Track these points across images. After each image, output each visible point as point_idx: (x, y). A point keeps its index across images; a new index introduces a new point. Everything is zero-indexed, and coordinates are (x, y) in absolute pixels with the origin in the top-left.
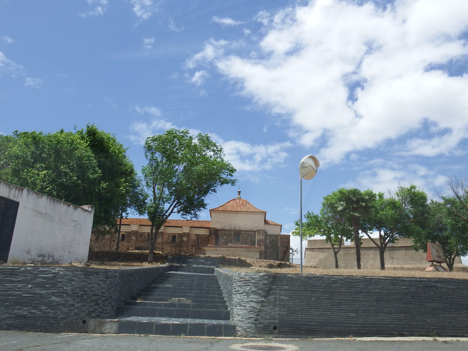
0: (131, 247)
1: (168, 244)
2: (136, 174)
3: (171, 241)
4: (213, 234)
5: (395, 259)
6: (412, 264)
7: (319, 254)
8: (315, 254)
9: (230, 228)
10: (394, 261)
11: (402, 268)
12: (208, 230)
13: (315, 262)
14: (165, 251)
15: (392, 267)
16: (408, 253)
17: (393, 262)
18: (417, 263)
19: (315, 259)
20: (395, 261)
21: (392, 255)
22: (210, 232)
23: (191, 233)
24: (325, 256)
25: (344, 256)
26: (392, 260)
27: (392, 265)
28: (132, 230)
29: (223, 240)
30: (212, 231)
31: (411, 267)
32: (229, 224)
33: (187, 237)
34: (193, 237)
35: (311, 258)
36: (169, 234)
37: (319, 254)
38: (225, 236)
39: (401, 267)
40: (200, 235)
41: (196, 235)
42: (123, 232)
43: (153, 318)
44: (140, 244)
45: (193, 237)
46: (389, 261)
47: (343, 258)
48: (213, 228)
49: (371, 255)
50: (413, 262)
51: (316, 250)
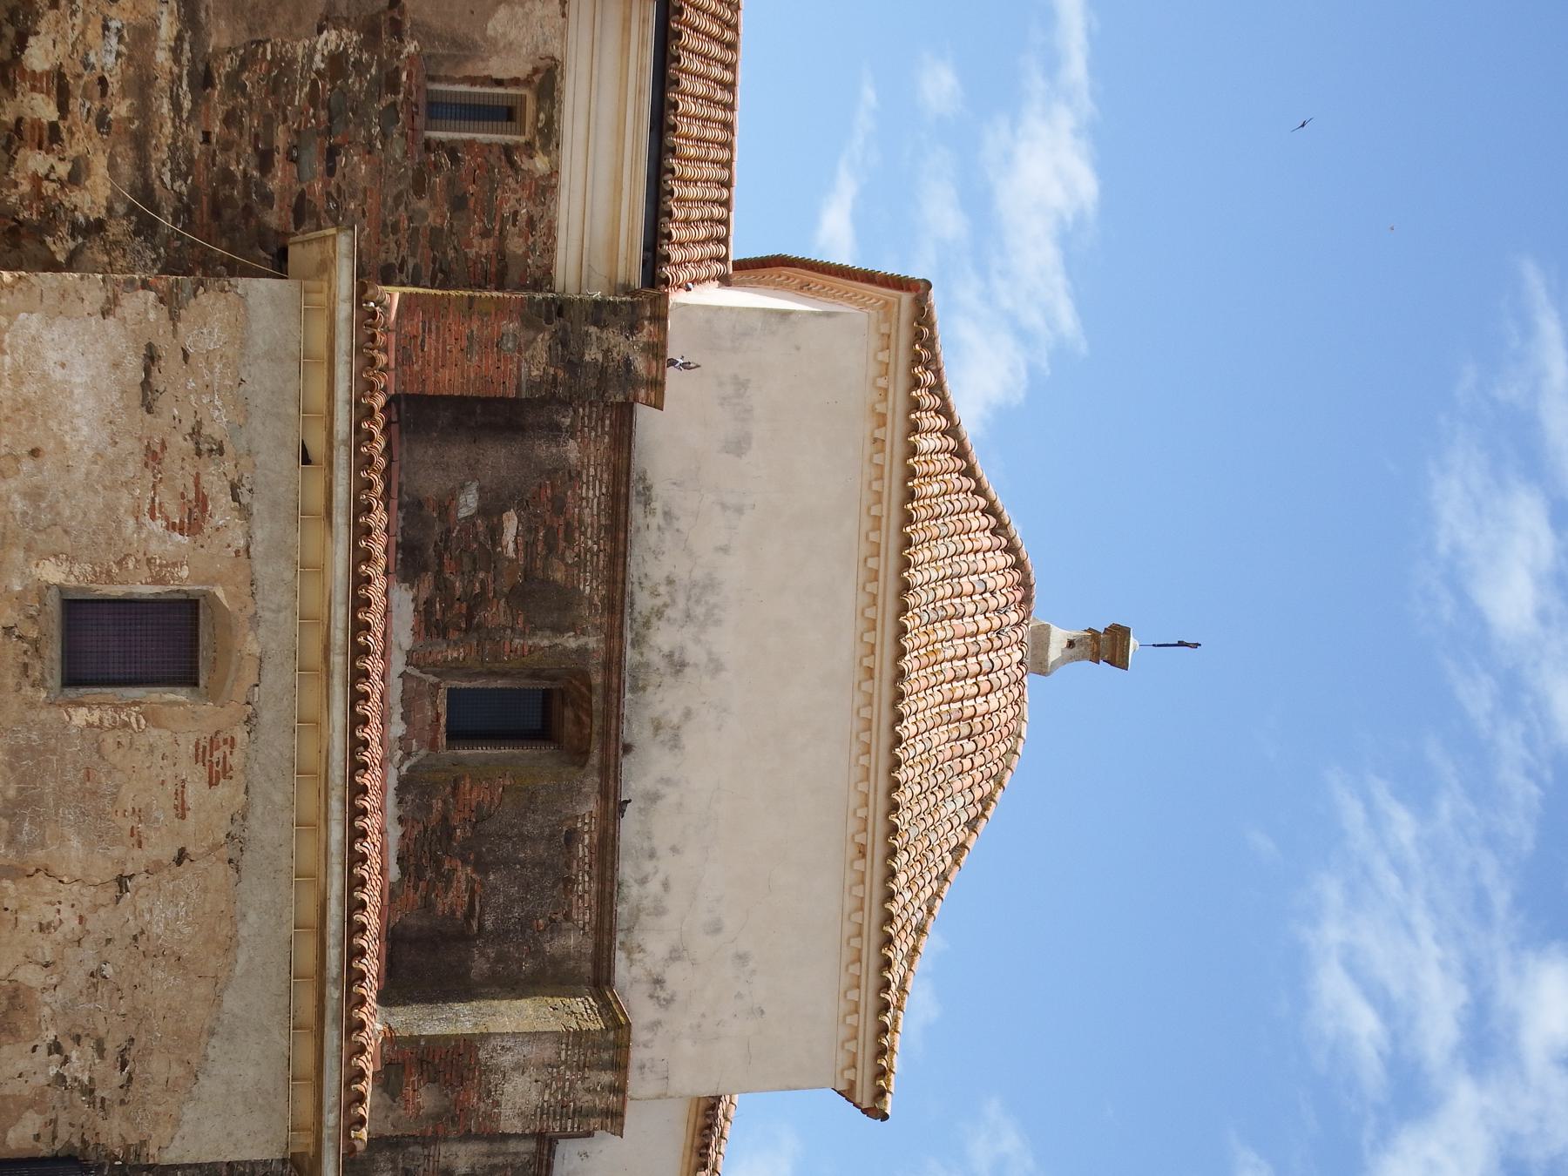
4: (573, 366)
9: (643, 602)
12: (630, 268)
29: (469, 503)
30: (614, 338)
32: (711, 585)
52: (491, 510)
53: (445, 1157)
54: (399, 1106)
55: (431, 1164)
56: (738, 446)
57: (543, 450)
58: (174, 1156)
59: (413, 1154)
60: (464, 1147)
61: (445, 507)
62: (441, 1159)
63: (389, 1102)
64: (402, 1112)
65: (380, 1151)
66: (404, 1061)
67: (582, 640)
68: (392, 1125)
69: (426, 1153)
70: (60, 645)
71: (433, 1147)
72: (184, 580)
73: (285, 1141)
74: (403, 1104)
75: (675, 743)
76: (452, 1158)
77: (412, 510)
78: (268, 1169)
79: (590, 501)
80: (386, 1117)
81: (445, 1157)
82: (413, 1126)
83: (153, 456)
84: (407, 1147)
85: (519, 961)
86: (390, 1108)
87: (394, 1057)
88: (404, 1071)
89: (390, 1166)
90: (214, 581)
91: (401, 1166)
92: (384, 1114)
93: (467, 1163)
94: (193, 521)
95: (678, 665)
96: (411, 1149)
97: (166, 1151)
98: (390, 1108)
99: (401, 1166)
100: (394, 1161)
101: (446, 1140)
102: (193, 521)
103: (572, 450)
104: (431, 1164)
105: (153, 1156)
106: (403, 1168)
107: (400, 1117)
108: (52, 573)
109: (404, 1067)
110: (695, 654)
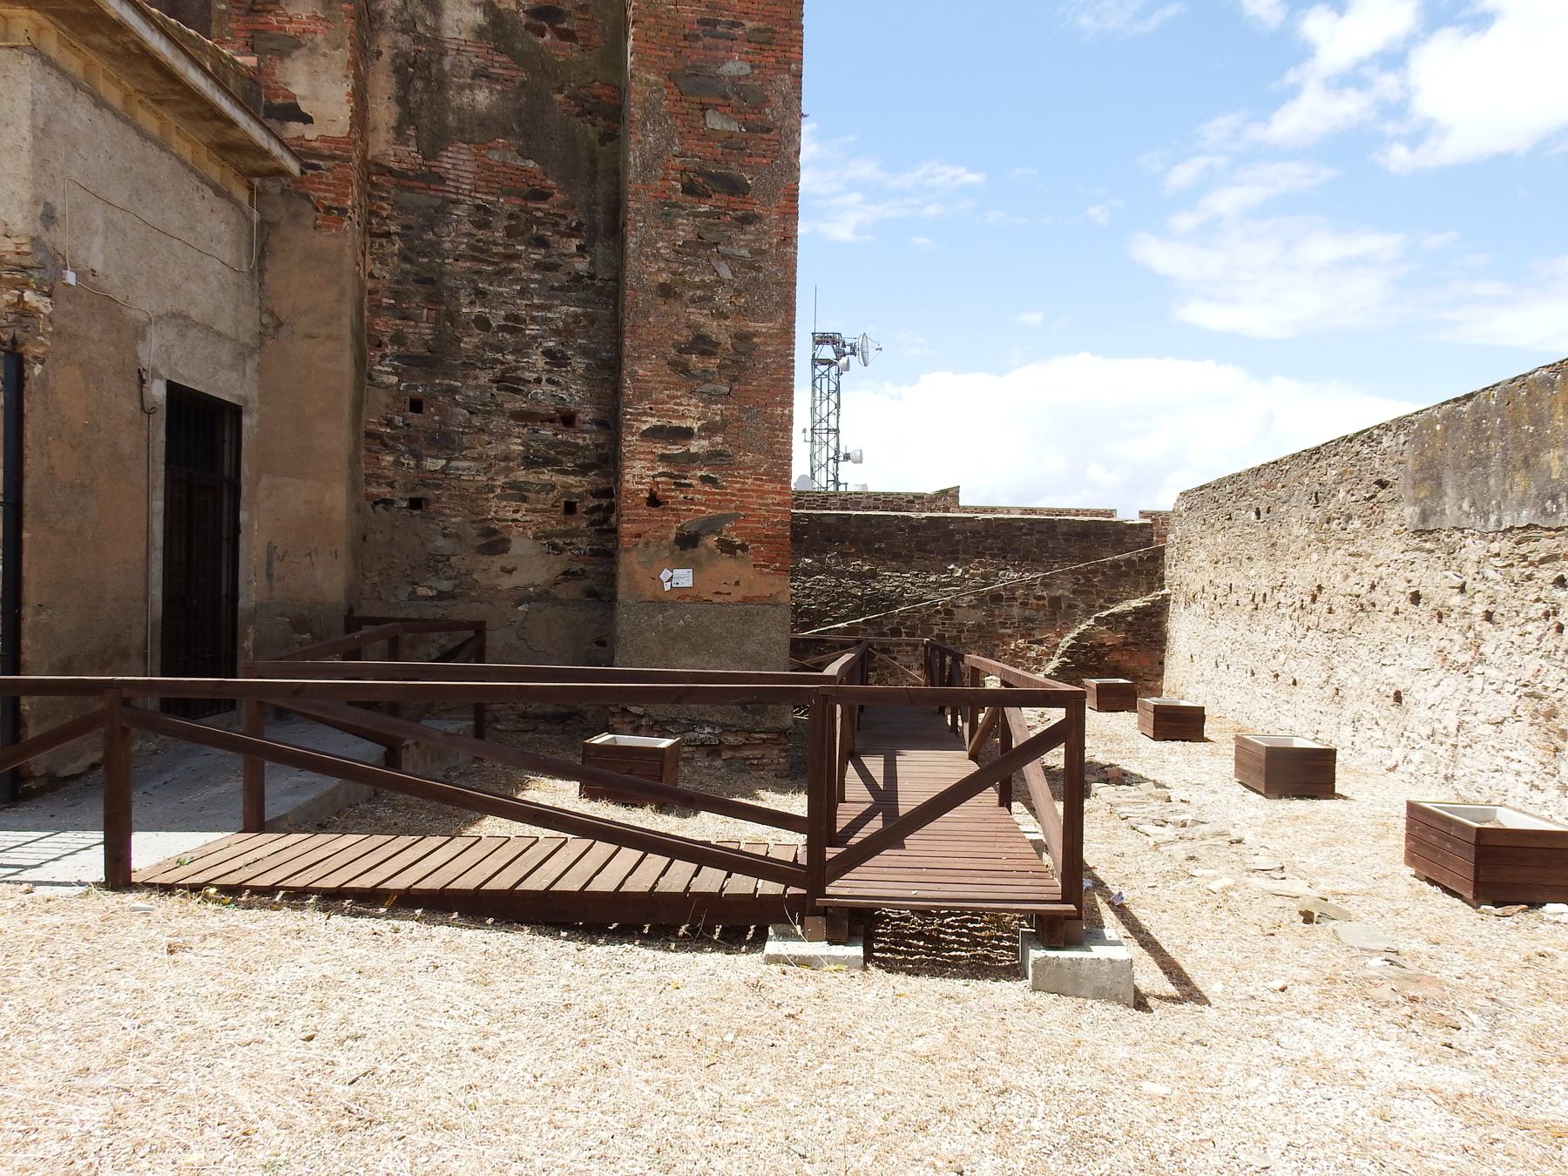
53: (460, 33)
54: (312, 40)
55: (469, 49)
58: (18, 217)
59: (454, 66)
60: (449, 12)
62: (463, 36)
63: (304, 51)
64: (319, 37)
65: (448, 101)
66: (248, 30)
67: (520, 163)
68: (335, 49)
69: (454, 53)
70: (162, 562)
71: (447, 45)
73: (8, 51)
74: (310, 36)
76: (461, 26)
78: (465, 220)
80: (325, 55)
81: (460, 33)
82: (339, 25)
84: (443, 71)
86: (313, 50)
87: (242, 42)
88: (263, 31)
89: (468, 92)
91: (469, 81)
92: (322, 59)
93: (468, 11)
96: (447, 67)
97: (10, 227)
98: (313, 50)
99: (469, 81)
100: (461, 88)
101: (437, 30)
104: (469, 49)
105: (18, 245)
106: (473, 78)
107: (326, 39)
109: (258, 31)
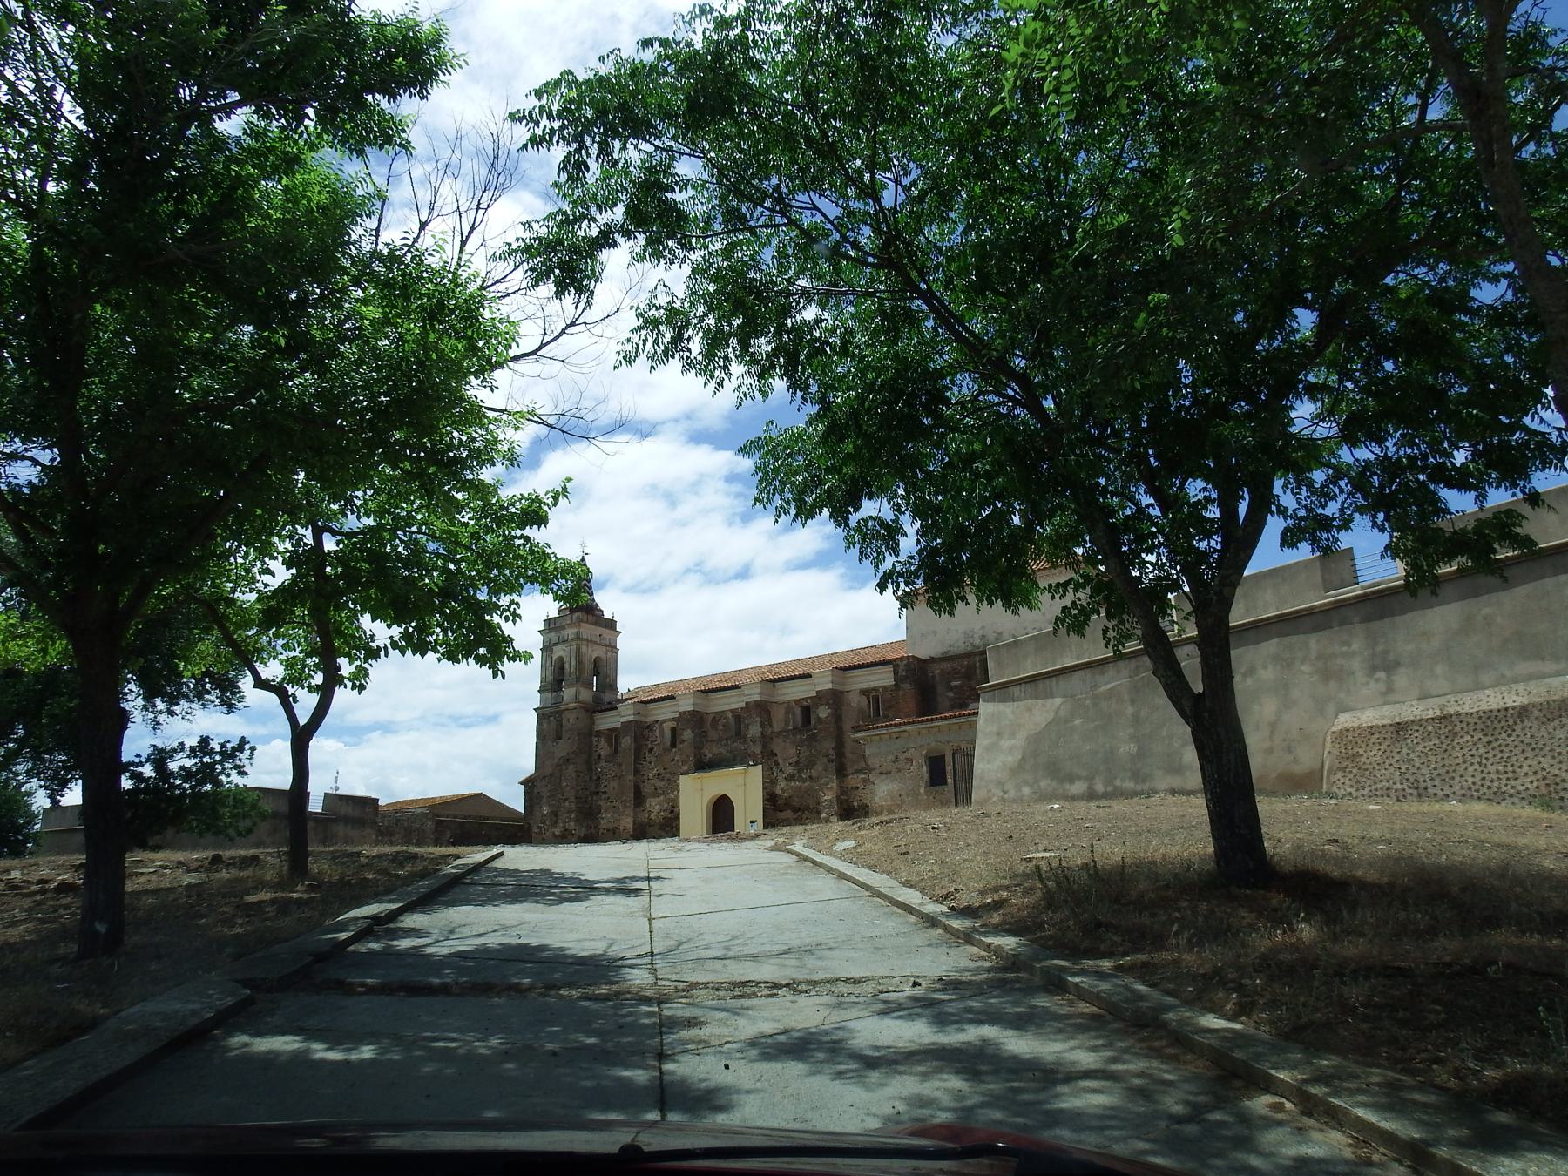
0: (684, 762)
1: (787, 737)
2: (243, 697)
3: (800, 725)
4: (907, 677)
5: (1402, 670)
6: (1516, 681)
7: (1029, 710)
8: (1013, 713)
9: (969, 648)
10: (1394, 678)
11: (1444, 717)
12: (890, 668)
13: (1011, 750)
14: (780, 761)
15: (1380, 723)
16: (1486, 611)
17: (1390, 689)
18: (1549, 667)
19: (1013, 735)
20: (1401, 679)
21: (1379, 648)
22: (896, 673)
23: (847, 688)
24: (1052, 716)
25: (1133, 701)
26: (1382, 675)
27: (1387, 710)
28: (682, 709)
29: (950, 694)
30: (901, 668)
31: (1510, 704)
32: (965, 633)
33: (828, 704)
34: (856, 701)
35: (999, 734)
36: (789, 702)
37: (1029, 710)
38: (955, 679)
39: (1438, 713)
40: (875, 689)
41: (865, 692)
42: (669, 720)
43: (1549, 1158)
44: (715, 750)
45: (856, 701)
46: (1367, 683)
47: (1130, 710)
48: (902, 659)
49: (1265, 667)
50: (1524, 667)
51: (1016, 690)
52: (951, 689)
56: (935, 633)
57: (938, 678)
61: (951, 699)
72: (922, 761)
75: (1001, 634)
77: (952, 708)
79: (947, 666)
83: (899, 770)
85: (956, 475)
90: (434, 928)
94: (910, 760)
95: (983, 637)
102: (910, 760)
103: (937, 672)
108: (922, 790)
110: (980, 633)
